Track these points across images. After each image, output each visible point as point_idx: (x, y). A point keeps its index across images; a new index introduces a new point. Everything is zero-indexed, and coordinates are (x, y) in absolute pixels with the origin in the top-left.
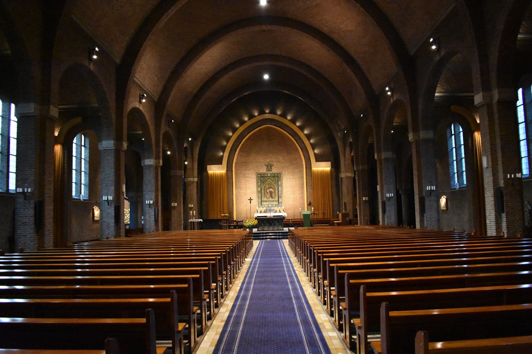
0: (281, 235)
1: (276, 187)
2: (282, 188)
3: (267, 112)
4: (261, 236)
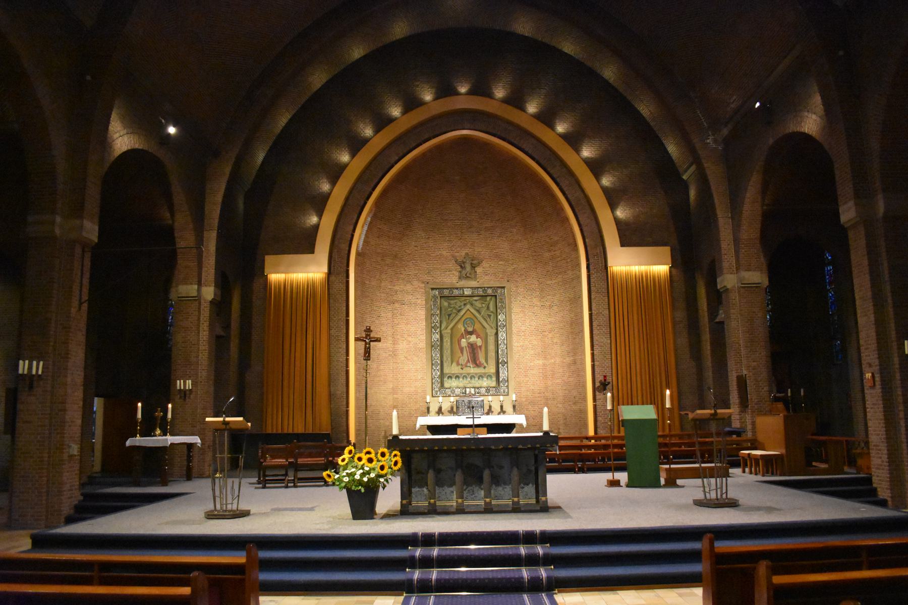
0: (547, 560)
1: (491, 332)
2: (509, 334)
3: (463, 90)
4: (412, 563)
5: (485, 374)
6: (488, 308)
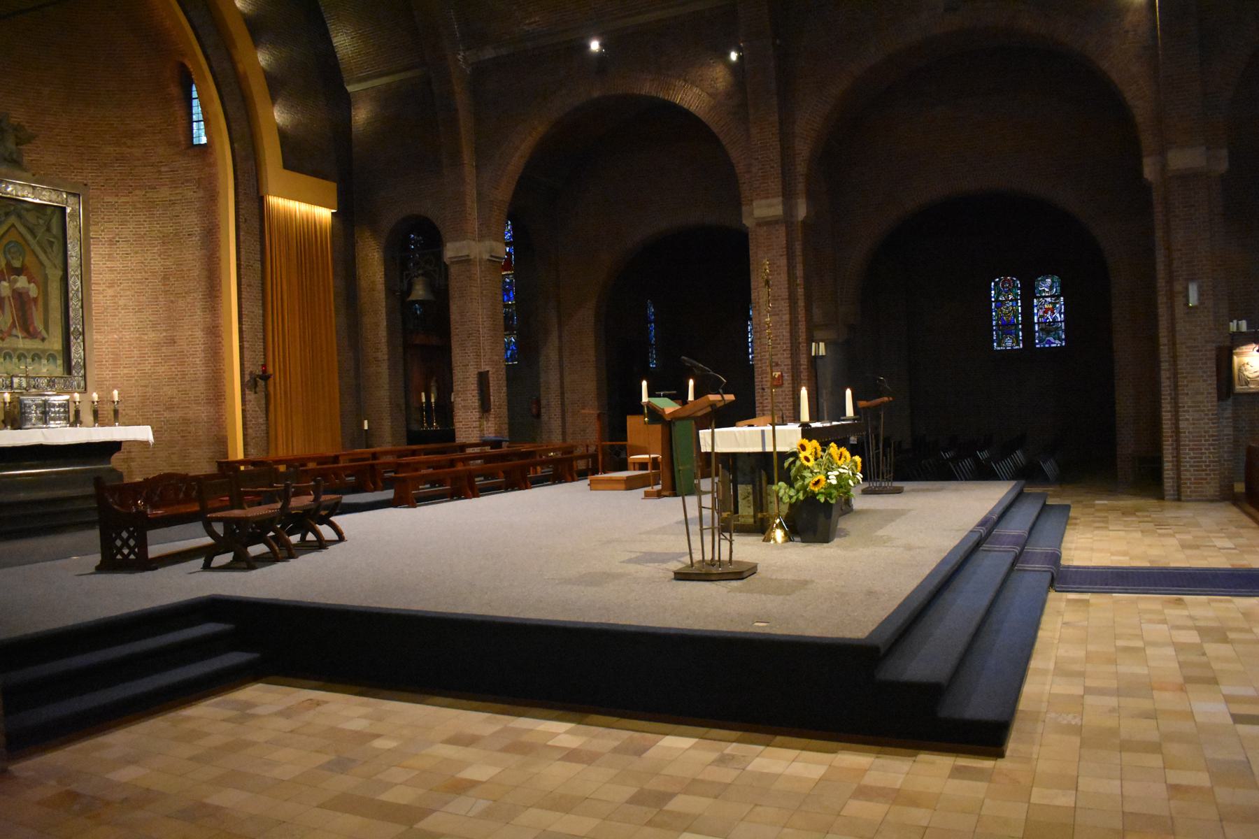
5: (44, 351)
6: (48, 229)
